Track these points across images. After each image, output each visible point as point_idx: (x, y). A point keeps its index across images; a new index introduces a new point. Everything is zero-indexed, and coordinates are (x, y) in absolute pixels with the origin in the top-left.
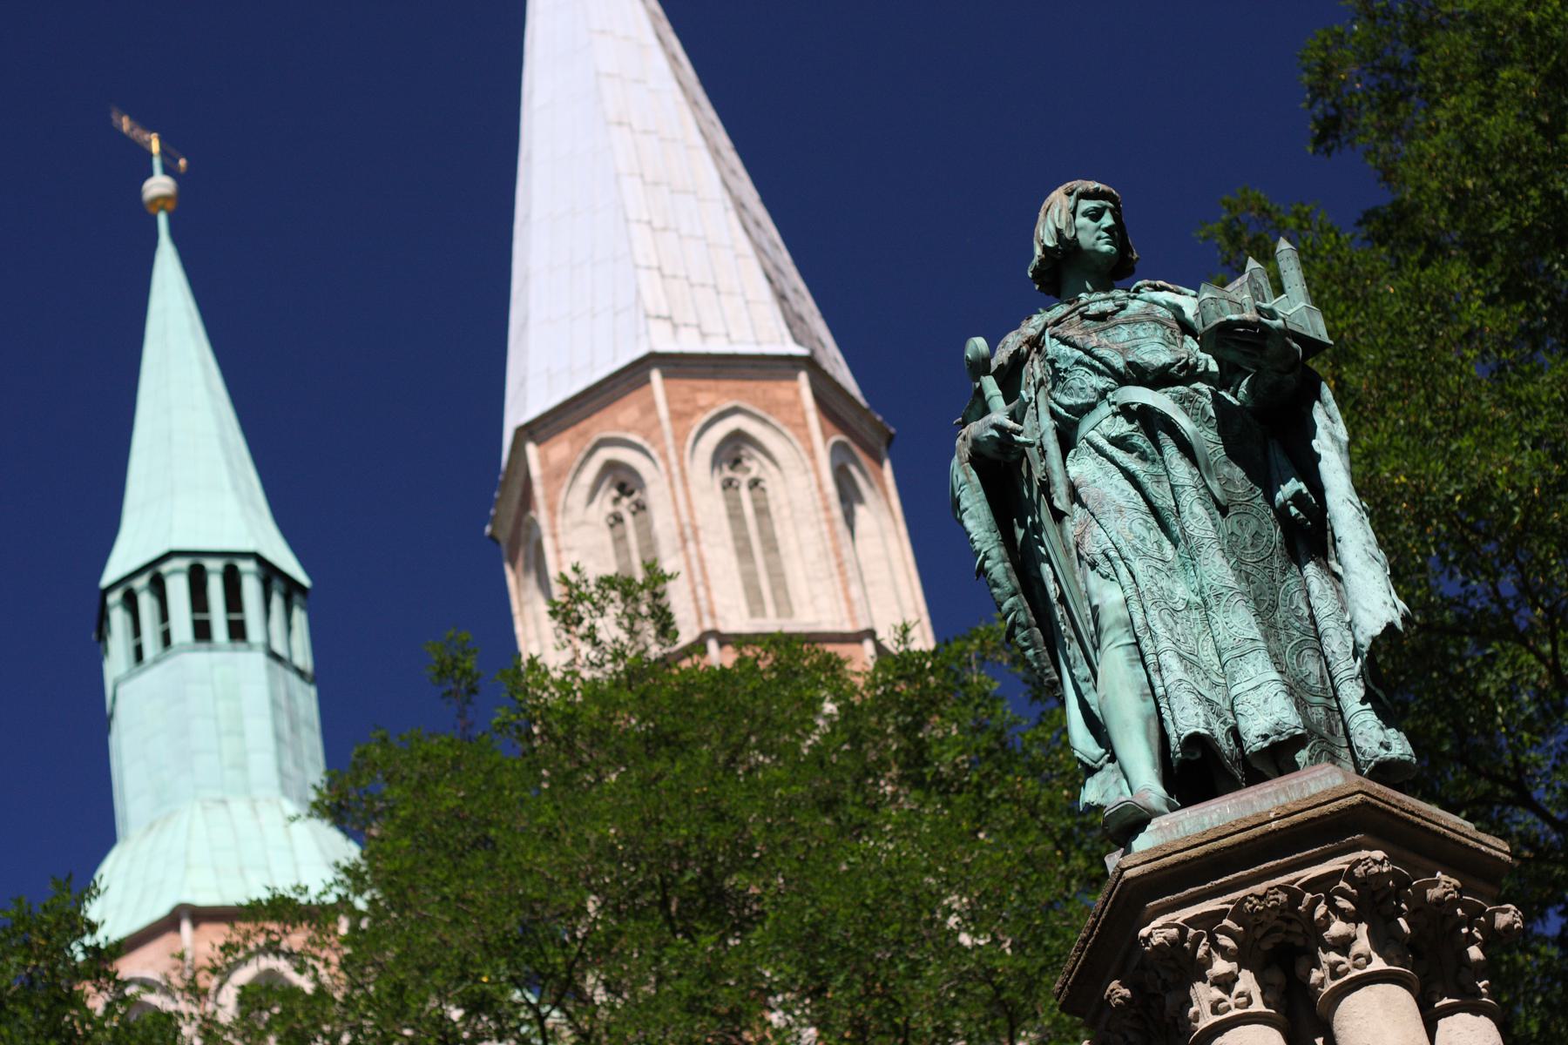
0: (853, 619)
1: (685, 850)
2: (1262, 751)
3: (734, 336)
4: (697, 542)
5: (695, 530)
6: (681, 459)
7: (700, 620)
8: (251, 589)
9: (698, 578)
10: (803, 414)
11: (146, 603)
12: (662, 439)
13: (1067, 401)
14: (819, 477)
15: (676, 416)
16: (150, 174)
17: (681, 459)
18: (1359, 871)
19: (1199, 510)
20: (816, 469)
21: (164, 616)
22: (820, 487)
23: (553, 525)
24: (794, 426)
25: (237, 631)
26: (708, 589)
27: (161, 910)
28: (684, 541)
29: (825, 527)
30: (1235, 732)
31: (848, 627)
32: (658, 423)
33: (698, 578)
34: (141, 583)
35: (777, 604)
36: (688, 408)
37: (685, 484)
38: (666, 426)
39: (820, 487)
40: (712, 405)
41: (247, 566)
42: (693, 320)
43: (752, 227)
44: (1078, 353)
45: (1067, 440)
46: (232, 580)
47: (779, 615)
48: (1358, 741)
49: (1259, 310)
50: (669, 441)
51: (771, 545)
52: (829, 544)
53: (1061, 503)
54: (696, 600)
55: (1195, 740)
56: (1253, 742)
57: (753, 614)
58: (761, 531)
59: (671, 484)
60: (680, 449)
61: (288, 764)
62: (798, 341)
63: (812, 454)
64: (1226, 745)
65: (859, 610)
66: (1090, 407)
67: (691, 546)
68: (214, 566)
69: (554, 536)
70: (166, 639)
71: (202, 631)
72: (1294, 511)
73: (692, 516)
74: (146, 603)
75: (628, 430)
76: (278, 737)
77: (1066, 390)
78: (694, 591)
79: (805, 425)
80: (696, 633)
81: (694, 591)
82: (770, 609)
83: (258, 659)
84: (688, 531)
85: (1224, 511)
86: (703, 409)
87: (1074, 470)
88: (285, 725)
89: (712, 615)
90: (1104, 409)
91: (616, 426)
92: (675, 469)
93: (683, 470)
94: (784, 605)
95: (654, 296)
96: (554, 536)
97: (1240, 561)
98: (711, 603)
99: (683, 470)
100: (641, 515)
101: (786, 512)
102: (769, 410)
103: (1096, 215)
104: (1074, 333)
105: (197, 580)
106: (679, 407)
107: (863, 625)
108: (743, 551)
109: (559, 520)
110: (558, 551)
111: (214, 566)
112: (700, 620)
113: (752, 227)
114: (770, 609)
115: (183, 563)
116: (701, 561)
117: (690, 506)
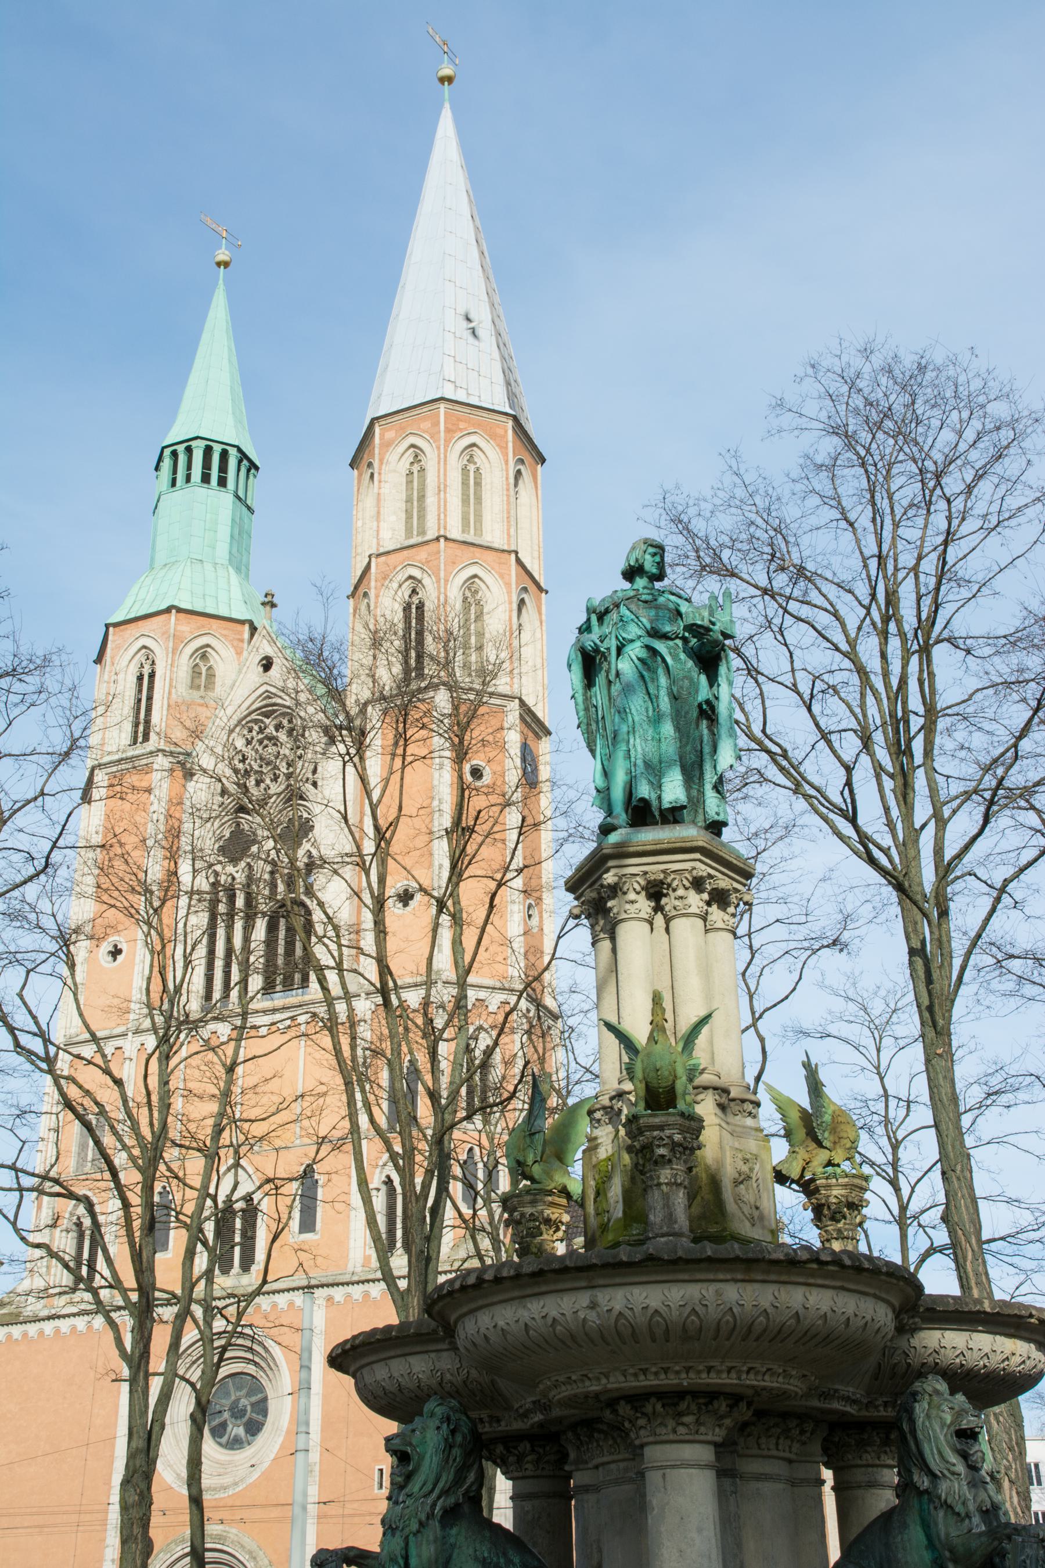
0: (509, 544)
1: (450, 1007)
2: (669, 809)
3: (482, 398)
4: (445, 493)
5: (445, 486)
6: (446, 451)
7: (439, 529)
8: (232, 463)
9: (442, 510)
10: (507, 443)
11: (182, 458)
12: (439, 440)
13: (624, 635)
14: (507, 474)
15: (448, 430)
16: (220, 248)
17: (446, 451)
18: (695, 873)
19: (666, 699)
20: (507, 470)
21: (189, 467)
22: (507, 479)
23: (380, 469)
24: (501, 447)
25: (222, 482)
26: (445, 516)
27: (164, 606)
28: (440, 491)
29: (505, 498)
30: (659, 798)
31: (506, 548)
32: (439, 432)
33: (442, 510)
34: (181, 449)
35: (475, 529)
36: (454, 428)
37: (445, 464)
38: (442, 434)
39: (507, 479)
40: (465, 429)
41: (233, 452)
42: (464, 386)
43: (501, 346)
44: (633, 617)
45: (619, 651)
46: (224, 455)
47: (475, 535)
48: (707, 809)
49: (711, 622)
50: (442, 442)
51: (479, 500)
52: (505, 507)
53: (612, 677)
54: (439, 519)
55: (643, 800)
56: (666, 805)
57: (463, 531)
58: (475, 493)
59: (439, 463)
60: (446, 446)
61: (234, 550)
62: (511, 407)
63: (507, 462)
64: (655, 804)
65: (513, 541)
66: (632, 641)
67: (442, 493)
68: (217, 449)
69: (380, 474)
70: (188, 479)
71: (206, 479)
72: (705, 707)
73: (445, 480)
74: (182, 458)
75: (424, 432)
76: (232, 537)
77: (624, 630)
78: (439, 515)
79: (507, 448)
80: (436, 535)
81: (439, 515)
82: (472, 531)
83: (230, 497)
84: (442, 486)
85: (676, 699)
86: (461, 430)
87: (620, 666)
88: (236, 531)
89: (445, 529)
90: (638, 644)
91: (419, 429)
92: (442, 456)
93: (445, 457)
94: (479, 531)
95: (449, 372)
96: (380, 474)
97: (678, 723)
98: (445, 522)
99: (445, 457)
100: (421, 473)
101: (488, 487)
102: (490, 436)
103: (654, 555)
104: (633, 607)
105: (208, 451)
106: (450, 426)
107: (513, 548)
108: (465, 501)
109: (384, 467)
110: (380, 482)
111: (217, 449)
112: (439, 529)
113: (501, 346)
114: (472, 531)
115: (202, 444)
116: (445, 502)
117: (445, 475)
